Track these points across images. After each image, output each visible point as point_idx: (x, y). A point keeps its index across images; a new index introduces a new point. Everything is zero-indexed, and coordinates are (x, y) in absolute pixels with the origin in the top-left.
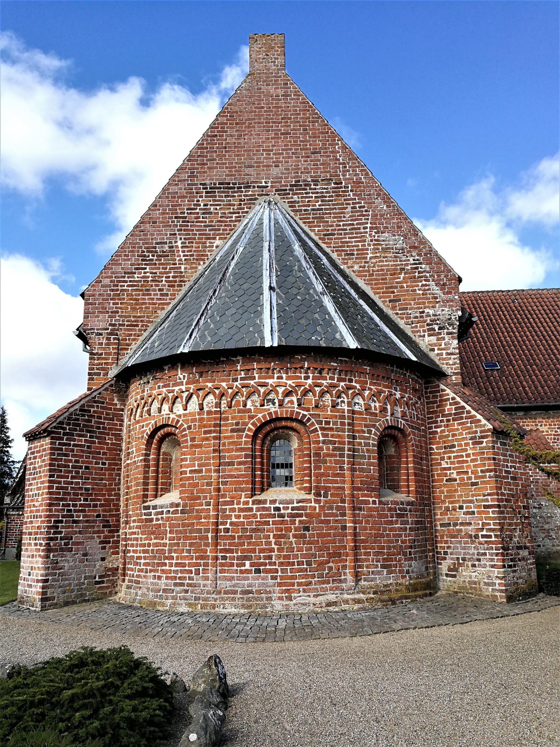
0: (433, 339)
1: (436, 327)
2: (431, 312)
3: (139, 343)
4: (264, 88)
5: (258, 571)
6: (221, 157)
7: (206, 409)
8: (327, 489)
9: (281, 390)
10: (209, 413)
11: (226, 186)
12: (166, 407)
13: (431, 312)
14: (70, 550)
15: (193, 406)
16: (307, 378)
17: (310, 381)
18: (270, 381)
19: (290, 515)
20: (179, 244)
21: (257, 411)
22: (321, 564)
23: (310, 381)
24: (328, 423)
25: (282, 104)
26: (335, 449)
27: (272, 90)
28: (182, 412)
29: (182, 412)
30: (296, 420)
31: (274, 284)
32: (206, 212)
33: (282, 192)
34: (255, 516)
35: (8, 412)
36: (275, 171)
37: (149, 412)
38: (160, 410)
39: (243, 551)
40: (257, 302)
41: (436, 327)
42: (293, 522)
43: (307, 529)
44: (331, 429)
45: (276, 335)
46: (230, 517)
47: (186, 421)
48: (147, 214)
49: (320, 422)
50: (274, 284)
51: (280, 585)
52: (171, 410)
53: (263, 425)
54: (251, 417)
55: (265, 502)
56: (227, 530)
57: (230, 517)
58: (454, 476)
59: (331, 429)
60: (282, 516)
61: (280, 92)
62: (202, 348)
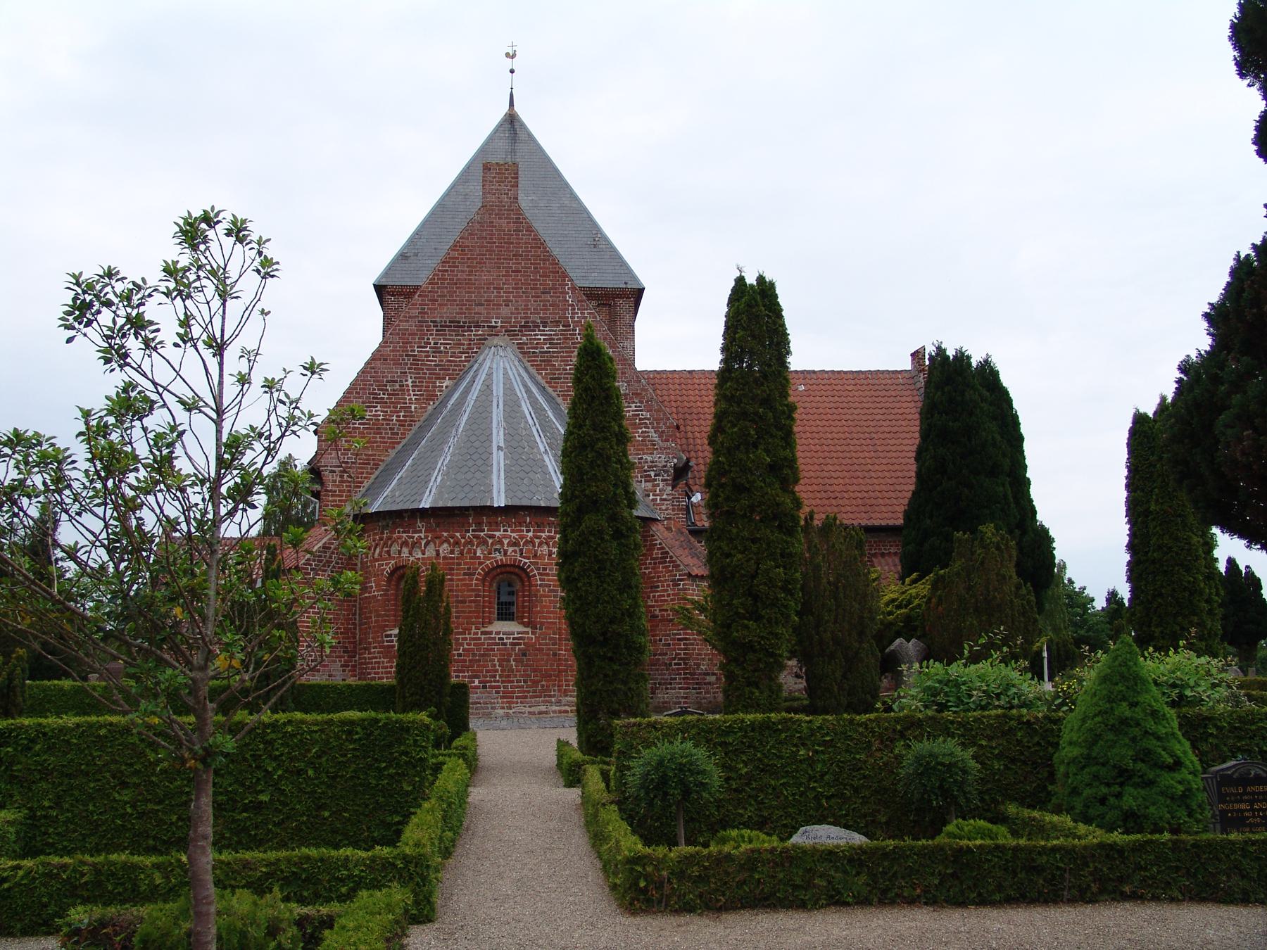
0: (649, 485)
1: (652, 474)
2: (649, 458)
3: (371, 481)
4: (497, 222)
5: (484, 687)
6: (452, 293)
7: (442, 555)
8: (542, 624)
9: (506, 541)
10: (445, 558)
11: (457, 325)
12: (405, 551)
13: (649, 458)
14: (318, 671)
15: (431, 552)
16: (528, 531)
17: (530, 534)
18: (497, 534)
19: (512, 644)
20: (410, 382)
21: (486, 558)
22: (535, 683)
23: (530, 534)
24: (545, 569)
25: (513, 239)
26: (550, 591)
27: (504, 223)
28: (420, 556)
29: (420, 556)
30: (519, 567)
31: (502, 444)
32: (437, 351)
33: (512, 334)
34: (483, 644)
35: (29, 427)
36: (505, 311)
37: (388, 552)
38: (400, 552)
39: (473, 671)
40: (487, 463)
41: (652, 474)
42: (513, 649)
43: (524, 655)
44: (548, 575)
45: (503, 495)
46: (462, 644)
47: (425, 564)
48: (378, 350)
49: (538, 569)
50: (502, 444)
51: (502, 698)
52: (410, 553)
53: (491, 570)
54: (481, 564)
55: (491, 633)
56: (460, 655)
57: (462, 644)
58: (657, 612)
59: (548, 575)
60: (505, 644)
61: (513, 226)
62: (440, 504)
